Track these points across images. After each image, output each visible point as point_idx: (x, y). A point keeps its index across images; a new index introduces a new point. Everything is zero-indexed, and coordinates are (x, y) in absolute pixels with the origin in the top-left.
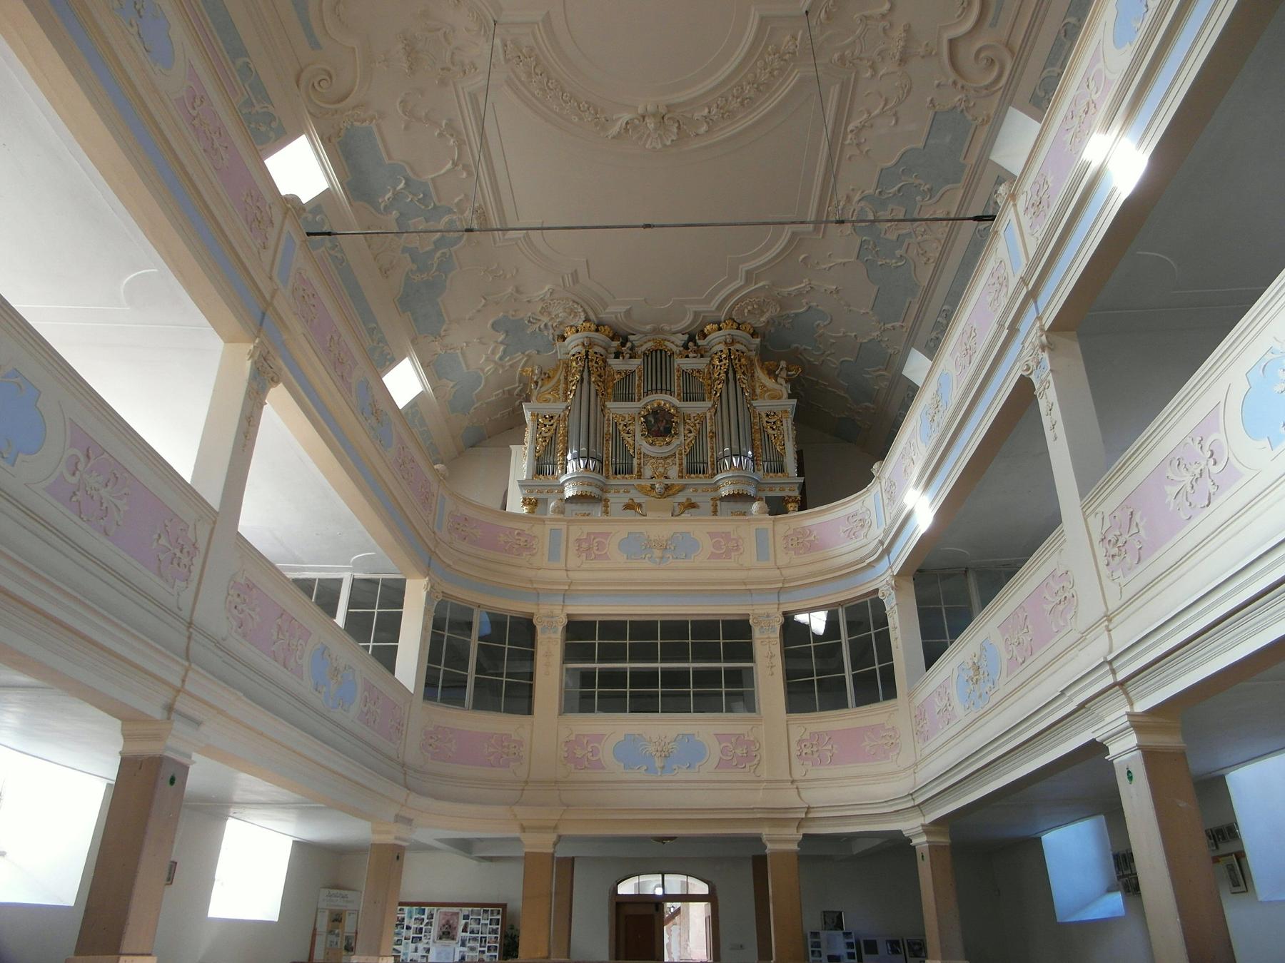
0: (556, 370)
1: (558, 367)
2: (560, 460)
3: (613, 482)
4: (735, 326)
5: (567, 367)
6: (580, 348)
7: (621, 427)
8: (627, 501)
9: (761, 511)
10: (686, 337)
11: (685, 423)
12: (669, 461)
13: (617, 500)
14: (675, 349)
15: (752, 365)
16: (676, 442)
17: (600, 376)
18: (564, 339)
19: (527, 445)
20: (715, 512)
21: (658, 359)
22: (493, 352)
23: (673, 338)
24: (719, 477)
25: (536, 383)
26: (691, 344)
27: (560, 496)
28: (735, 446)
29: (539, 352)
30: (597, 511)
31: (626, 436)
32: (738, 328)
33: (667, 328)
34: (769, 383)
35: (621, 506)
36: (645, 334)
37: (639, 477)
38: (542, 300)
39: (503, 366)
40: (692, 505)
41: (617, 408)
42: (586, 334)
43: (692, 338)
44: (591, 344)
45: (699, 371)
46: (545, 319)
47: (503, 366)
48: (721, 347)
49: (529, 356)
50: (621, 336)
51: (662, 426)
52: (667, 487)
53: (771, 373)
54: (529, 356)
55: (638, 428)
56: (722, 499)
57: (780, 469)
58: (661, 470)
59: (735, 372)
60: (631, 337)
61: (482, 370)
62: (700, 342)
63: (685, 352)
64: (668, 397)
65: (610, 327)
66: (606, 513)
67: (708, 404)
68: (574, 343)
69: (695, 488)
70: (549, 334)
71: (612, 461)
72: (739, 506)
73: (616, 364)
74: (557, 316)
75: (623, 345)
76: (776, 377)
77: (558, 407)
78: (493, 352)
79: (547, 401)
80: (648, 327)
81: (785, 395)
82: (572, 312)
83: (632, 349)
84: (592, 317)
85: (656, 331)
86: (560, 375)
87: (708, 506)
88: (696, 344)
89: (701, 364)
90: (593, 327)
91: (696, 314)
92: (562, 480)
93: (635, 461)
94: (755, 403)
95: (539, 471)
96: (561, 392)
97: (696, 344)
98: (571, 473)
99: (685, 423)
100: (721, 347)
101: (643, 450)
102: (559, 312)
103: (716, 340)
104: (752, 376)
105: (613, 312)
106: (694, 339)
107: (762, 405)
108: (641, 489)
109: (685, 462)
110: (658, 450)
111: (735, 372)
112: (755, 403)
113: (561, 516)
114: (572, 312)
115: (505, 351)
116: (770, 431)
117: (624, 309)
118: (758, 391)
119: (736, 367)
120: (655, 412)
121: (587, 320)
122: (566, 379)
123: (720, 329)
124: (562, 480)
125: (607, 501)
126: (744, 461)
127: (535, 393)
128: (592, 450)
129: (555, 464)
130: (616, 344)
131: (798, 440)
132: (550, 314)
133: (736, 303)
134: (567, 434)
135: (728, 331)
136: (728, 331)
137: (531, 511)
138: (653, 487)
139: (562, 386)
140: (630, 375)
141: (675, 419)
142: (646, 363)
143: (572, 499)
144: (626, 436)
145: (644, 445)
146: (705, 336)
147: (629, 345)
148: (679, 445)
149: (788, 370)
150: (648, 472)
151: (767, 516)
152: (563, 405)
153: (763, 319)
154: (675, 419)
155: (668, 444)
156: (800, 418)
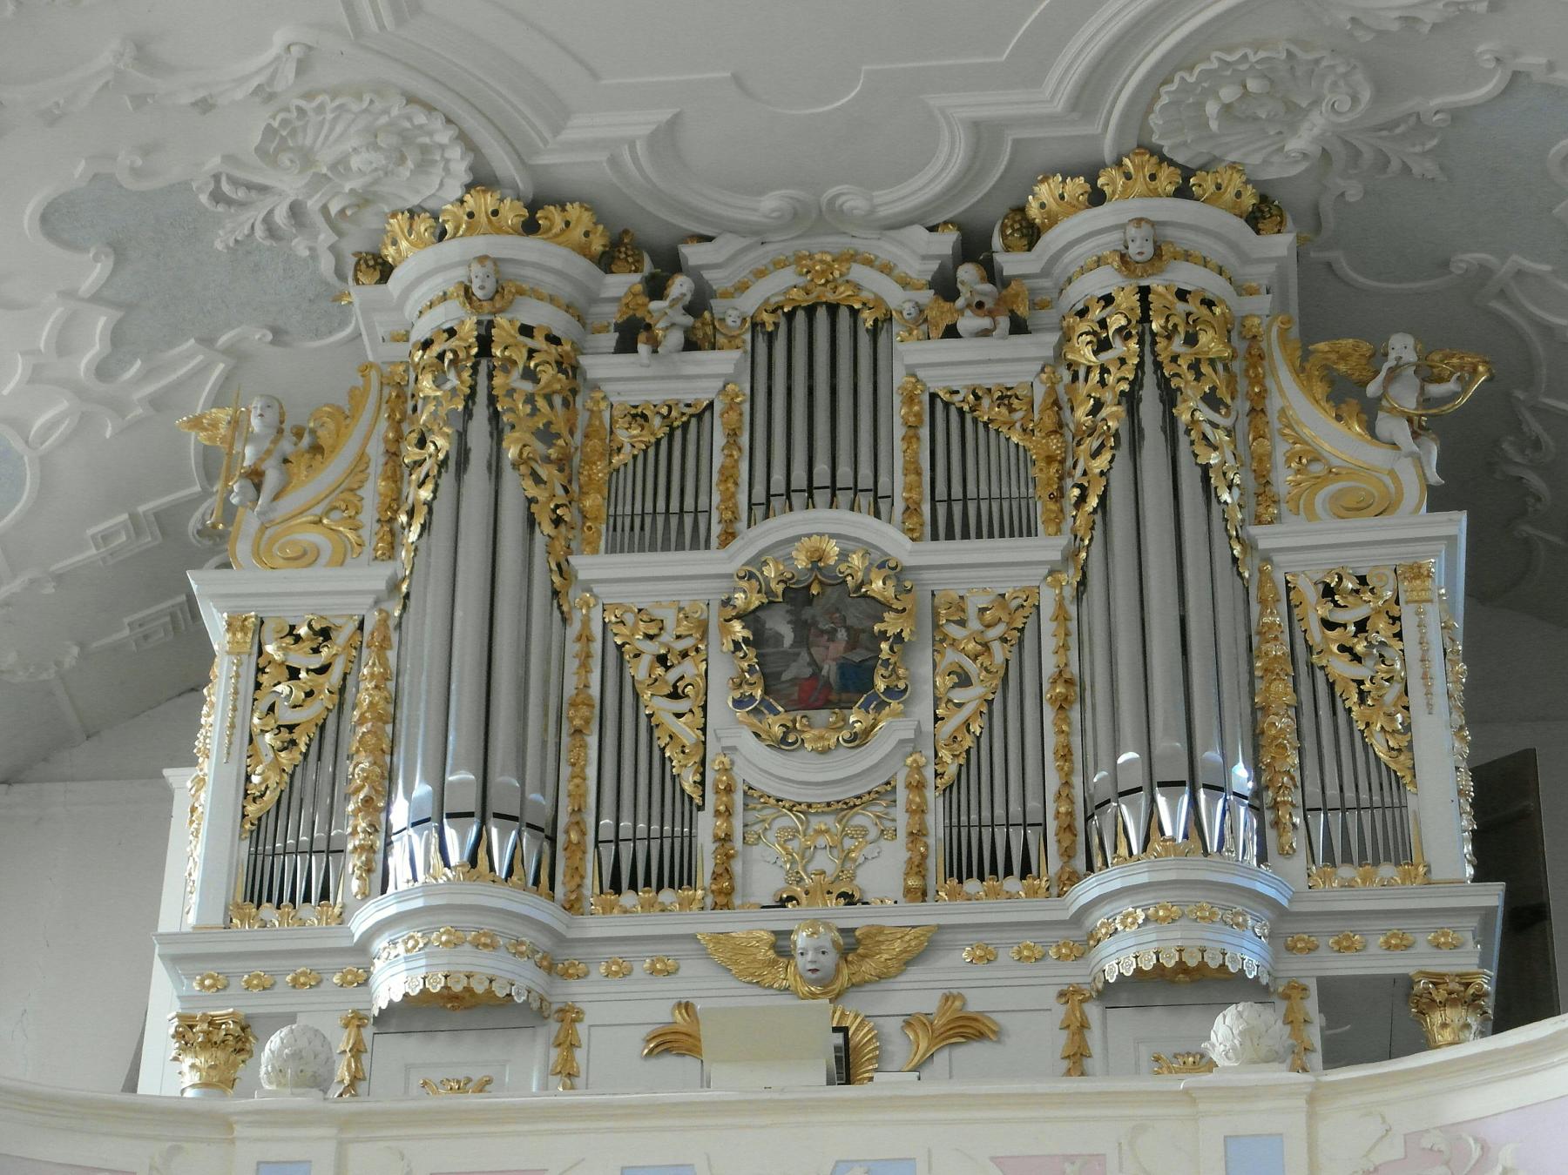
0: (343, 418)
1: (356, 397)
2: (353, 829)
3: (596, 926)
4: (1167, 179)
5: (401, 400)
6: (451, 312)
7: (640, 670)
8: (662, 1013)
9: (1255, 1052)
10: (947, 242)
11: (941, 640)
12: (863, 819)
13: (618, 1012)
14: (895, 297)
15: (1257, 357)
16: (893, 728)
17: (547, 435)
18: (384, 270)
19: (207, 767)
20: (1077, 1059)
21: (819, 341)
22: (64, 345)
23: (885, 249)
24: (1089, 889)
25: (255, 477)
26: (968, 273)
27: (351, 1000)
28: (1169, 744)
29: (279, 335)
30: (523, 1066)
31: (662, 707)
32: (1183, 192)
33: (854, 202)
34: (1337, 439)
35: (634, 1042)
36: (758, 234)
37: (724, 898)
38: (265, 94)
39: (118, 406)
40: (966, 1029)
41: (627, 583)
42: (480, 244)
43: (973, 247)
44: (503, 291)
45: (1006, 398)
46: (289, 184)
47: (118, 406)
48: (1106, 280)
49: (238, 356)
50: (645, 253)
51: (830, 656)
52: (850, 945)
53: (1349, 395)
54: (238, 356)
55: (722, 670)
56: (1113, 993)
57: (1393, 845)
58: (825, 862)
59: (1169, 397)
60: (693, 254)
61: (20, 427)
62: (1011, 263)
63: (941, 313)
64: (860, 524)
65: (589, 204)
66: (568, 1074)
67: (1046, 547)
68: (428, 286)
69: (988, 947)
70: (318, 251)
71: (607, 833)
72: (1156, 1026)
73: (623, 379)
74: (340, 166)
75: (656, 288)
76: (1369, 413)
77: (349, 587)
78: (64, 345)
79: (305, 557)
80: (770, 203)
81: (1413, 493)
82: (408, 148)
83: (697, 306)
84: (503, 163)
85: (813, 217)
86: (368, 435)
87: (1036, 1029)
88: (991, 273)
89: (1014, 362)
90: (512, 213)
91: (983, 134)
92: (360, 923)
93: (706, 826)
94: (1266, 538)
95: (261, 888)
96: (369, 516)
97: (991, 273)
98: (402, 906)
99: (941, 640)
100: (1106, 280)
101: (742, 774)
102: (349, 150)
103: (1081, 249)
104: (1257, 411)
105: (598, 139)
106: (981, 252)
107: (1302, 546)
108: (728, 956)
109: (936, 822)
110: (817, 767)
111: (1169, 397)
112: (1266, 538)
113: (307, 1100)
114: (408, 148)
115: (117, 337)
116: (1341, 667)
117: (640, 123)
118: (1284, 479)
119: (1168, 366)
120: (797, 596)
121: (481, 180)
122: (394, 455)
123: (1097, 198)
124: (360, 923)
125: (569, 1016)
126: (1212, 812)
127: (249, 522)
128: (503, 778)
129: (334, 851)
130: (622, 283)
131: (1479, 708)
132: (306, 158)
133: (1161, 76)
134: (389, 714)
135: (1136, 207)
136: (1136, 207)
137: (220, 1081)
138: (782, 946)
139: (374, 489)
140: (685, 426)
141: (891, 624)
142: (760, 370)
143: (411, 1015)
144: (662, 707)
145: (743, 747)
146: (1031, 234)
147: (680, 286)
148: (911, 745)
149: (1428, 375)
150: (763, 873)
151: (1280, 1075)
152: (376, 577)
153: (1298, 143)
154: (891, 624)
155: (859, 739)
156: (1494, 583)
